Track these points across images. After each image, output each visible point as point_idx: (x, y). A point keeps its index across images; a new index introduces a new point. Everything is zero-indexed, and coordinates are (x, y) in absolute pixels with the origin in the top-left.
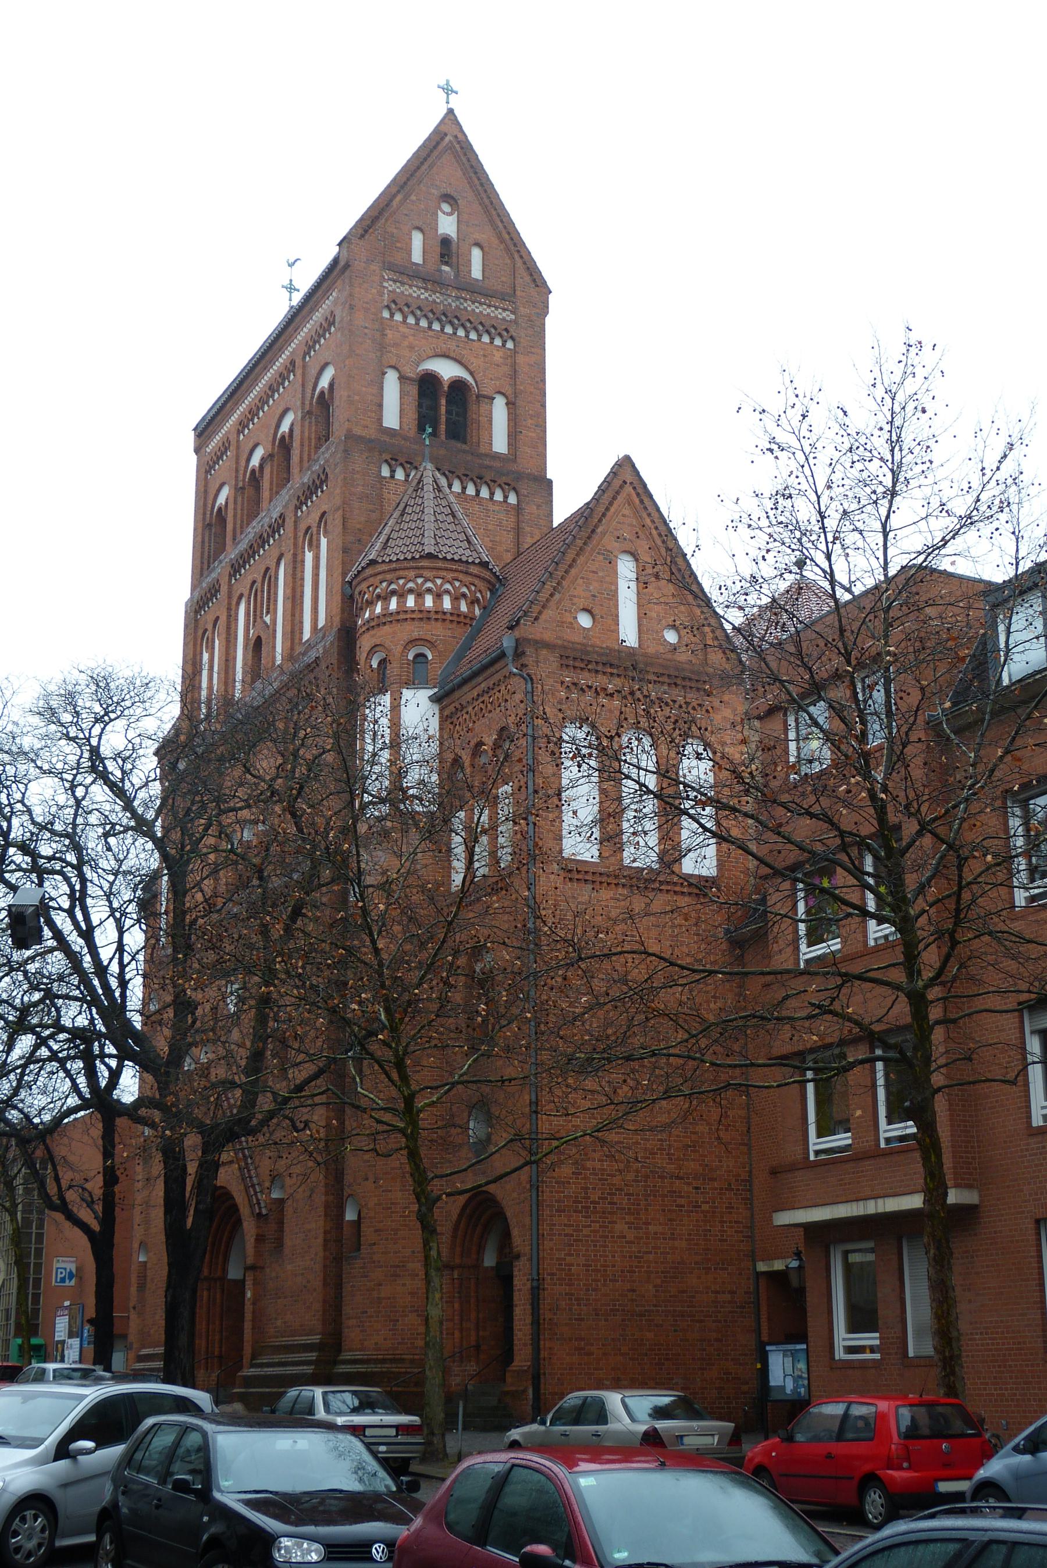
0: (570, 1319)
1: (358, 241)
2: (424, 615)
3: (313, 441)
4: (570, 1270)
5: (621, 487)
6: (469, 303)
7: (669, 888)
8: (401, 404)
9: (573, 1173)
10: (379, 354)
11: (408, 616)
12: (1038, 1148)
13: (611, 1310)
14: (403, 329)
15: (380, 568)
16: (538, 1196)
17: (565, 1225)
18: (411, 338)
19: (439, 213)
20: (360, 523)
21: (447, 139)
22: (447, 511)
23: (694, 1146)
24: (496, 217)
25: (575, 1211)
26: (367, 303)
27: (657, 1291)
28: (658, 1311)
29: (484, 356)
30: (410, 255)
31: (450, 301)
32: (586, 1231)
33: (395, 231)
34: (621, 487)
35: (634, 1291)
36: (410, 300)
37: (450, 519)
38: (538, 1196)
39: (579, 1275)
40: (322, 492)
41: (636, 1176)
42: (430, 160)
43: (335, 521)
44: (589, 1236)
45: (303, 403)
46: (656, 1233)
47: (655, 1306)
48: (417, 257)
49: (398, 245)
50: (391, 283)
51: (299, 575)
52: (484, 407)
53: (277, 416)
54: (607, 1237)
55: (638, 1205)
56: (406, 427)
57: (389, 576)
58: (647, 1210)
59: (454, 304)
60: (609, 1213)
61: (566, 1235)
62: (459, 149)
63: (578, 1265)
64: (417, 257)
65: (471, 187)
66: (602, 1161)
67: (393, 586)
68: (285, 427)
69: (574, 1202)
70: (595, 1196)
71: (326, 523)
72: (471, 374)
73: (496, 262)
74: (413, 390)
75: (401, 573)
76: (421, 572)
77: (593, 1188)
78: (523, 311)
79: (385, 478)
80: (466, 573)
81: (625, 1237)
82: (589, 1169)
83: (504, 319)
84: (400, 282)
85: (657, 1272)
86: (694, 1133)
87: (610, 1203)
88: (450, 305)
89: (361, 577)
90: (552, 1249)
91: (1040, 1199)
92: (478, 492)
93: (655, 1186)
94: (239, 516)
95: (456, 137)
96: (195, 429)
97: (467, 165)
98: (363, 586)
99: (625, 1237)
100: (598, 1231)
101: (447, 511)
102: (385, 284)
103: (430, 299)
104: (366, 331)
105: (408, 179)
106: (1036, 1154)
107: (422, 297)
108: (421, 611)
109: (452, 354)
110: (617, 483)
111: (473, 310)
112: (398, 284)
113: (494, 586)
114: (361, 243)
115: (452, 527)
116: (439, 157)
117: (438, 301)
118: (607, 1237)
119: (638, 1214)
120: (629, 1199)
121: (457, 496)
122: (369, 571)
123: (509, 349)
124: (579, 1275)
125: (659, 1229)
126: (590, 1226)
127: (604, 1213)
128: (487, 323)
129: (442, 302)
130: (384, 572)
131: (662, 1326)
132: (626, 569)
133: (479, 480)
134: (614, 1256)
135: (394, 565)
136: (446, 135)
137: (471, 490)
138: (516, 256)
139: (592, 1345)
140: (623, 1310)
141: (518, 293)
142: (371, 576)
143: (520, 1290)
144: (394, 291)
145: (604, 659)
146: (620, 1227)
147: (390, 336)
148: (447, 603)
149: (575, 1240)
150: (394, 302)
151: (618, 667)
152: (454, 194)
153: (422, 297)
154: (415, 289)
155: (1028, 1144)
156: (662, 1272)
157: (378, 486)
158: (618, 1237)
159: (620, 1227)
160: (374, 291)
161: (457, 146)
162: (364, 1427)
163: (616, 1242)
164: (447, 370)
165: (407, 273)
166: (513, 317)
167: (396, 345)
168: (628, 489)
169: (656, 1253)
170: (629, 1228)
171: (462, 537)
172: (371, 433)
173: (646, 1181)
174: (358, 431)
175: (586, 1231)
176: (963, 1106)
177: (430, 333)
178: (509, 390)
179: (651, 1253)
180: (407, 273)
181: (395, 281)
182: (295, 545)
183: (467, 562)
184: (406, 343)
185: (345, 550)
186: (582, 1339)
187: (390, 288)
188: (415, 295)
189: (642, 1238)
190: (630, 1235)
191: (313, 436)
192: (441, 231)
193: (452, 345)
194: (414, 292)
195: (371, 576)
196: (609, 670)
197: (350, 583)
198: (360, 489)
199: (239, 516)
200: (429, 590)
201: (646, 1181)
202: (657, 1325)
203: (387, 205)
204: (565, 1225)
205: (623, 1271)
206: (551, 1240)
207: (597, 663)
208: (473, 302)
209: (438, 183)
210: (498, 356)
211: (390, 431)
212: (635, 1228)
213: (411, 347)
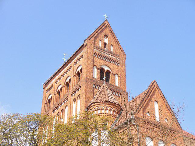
2: (106, 114)
3: (76, 81)
5: (154, 87)
11: (102, 114)
15: (96, 104)
21: (106, 25)
34: (154, 87)
40: (80, 89)
43: (83, 97)
45: (73, 74)
48: (100, 45)
51: (71, 109)
53: (66, 78)
57: (98, 106)
67: (99, 108)
68: (50, 98)
71: (63, 111)
72: (111, 69)
74: (99, 71)
75: (101, 105)
83: (117, 60)
89: (91, 106)
94: (54, 100)
98: (91, 108)
108: (106, 114)
109: (107, 65)
110: (153, 86)
128: (114, 60)
130: (97, 105)
132: (156, 106)
135: (99, 103)
142: (94, 106)
148: (111, 112)
150: (96, 53)
151: (156, 125)
165: (98, 48)
168: (155, 87)
172: (91, 78)
174: (88, 77)
180: (98, 48)
181: (96, 49)
182: (71, 103)
183: (114, 103)
185: (86, 102)
191: (76, 80)
195: (94, 106)
197: (87, 108)
199: (54, 100)
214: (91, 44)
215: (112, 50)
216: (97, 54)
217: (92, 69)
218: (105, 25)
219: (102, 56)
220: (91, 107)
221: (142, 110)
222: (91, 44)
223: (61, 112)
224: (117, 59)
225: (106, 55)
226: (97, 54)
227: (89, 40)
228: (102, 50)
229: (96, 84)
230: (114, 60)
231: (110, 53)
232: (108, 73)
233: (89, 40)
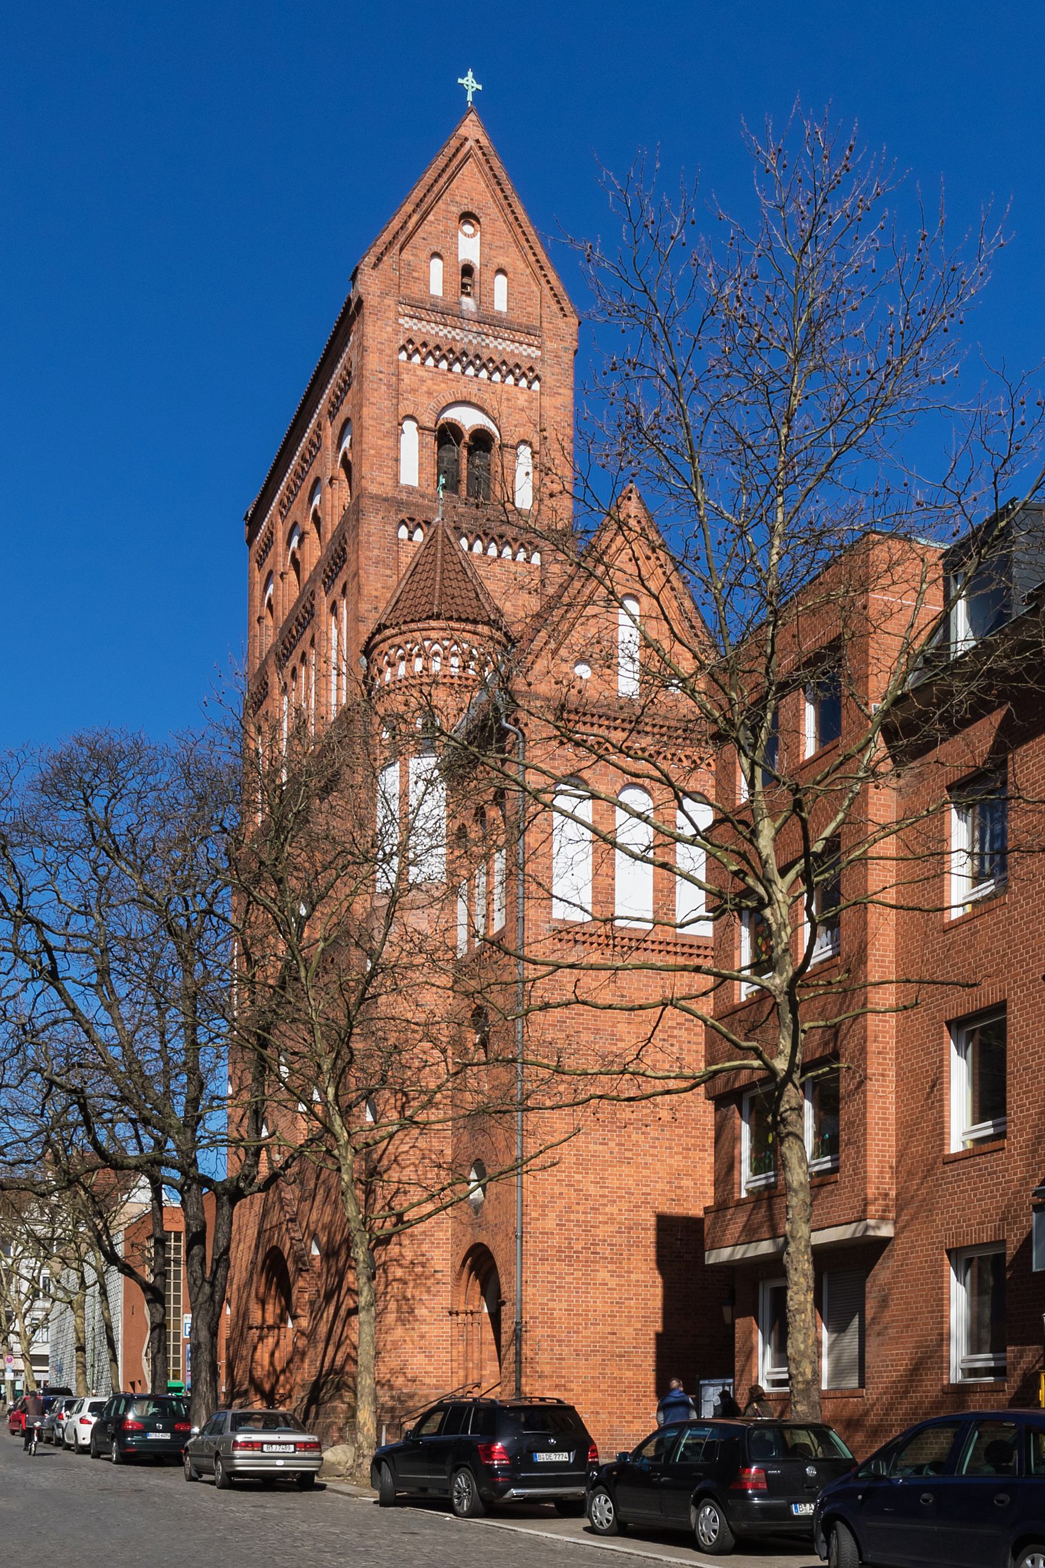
0: (551, 1359)
1: (371, 272)
4: (552, 1314)
6: (492, 338)
7: (661, 947)
8: (420, 458)
9: (557, 1225)
10: (395, 401)
12: (953, 1176)
13: (591, 1351)
14: (421, 372)
16: (522, 1246)
17: (548, 1273)
18: (430, 382)
19: (460, 234)
20: (376, 590)
21: (468, 145)
22: (458, 568)
23: (679, 1200)
24: (520, 236)
25: (558, 1260)
26: (381, 343)
27: (637, 1334)
28: (637, 1352)
29: (508, 400)
30: (428, 286)
31: (470, 337)
32: (569, 1279)
33: (411, 258)
35: (614, 1334)
36: (427, 338)
37: (460, 577)
38: (522, 1246)
39: (560, 1319)
41: (620, 1228)
42: (449, 171)
44: (572, 1283)
46: (637, 1281)
47: (634, 1348)
48: (436, 288)
49: (415, 274)
50: (407, 319)
52: (508, 457)
54: (589, 1284)
55: (621, 1254)
56: (425, 484)
58: (629, 1259)
59: (475, 342)
60: (592, 1262)
61: (549, 1282)
62: (481, 156)
63: (560, 1310)
64: (436, 288)
65: (495, 202)
66: (586, 1213)
69: (558, 1251)
70: (578, 1247)
72: (494, 420)
73: (522, 290)
74: (430, 440)
76: (428, 633)
77: (577, 1239)
78: (550, 345)
79: (403, 540)
80: (475, 633)
81: (607, 1284)
82: (573, 1221)
84: (416, 318)
85: (638, 1317)
86: (680, 1187)
87: (592, 1253)
88: (470, 342)
90: (534, 1295)
91: (951, 1229)
92: (500, 553)
93: (638, 1237)
95: (478, 141)
96: (245, 519)
97: (490, 175)
99: (607, 1284)
100: (581, 1279)
101: (458, 568)
102: (401, 321)
103: (450, 336)
104: (381, 376)
105: (425, 196)
106: (951, 1183)
107: (441, 334)
109: (474, 400)
111: (496, 347)
112: (415, 320)
113: (505, 647)
114: (374, 273)
115: (462, 585)
116: (459, 167)
117: (458, 338)
118: (589, 1284)
119: (620, 1263)
120: (612, 1250)
121: (479, 557)
122: (378, 638)
123: (534, 391)
124: (560, 1319)
125: (641, 1277)
126: (573, 1274)
127: (586, 1262)
128: (511, 362)
129: (462, 339)
131: (641, 1366)
133: (502, 540)
134: (595, 1302)
136: (466, 139)
137: (493, 551)
138: (543, 281)
139: (572, 1382)
140: (603, 1351)
141: (544, 325)
143: (506, 1332)
144: (410, 329)
145: (601, 711)
146: (603, 1275)
147: (406, 381)
149: (558, 1287)
152: (476, 212)
153: (441, 334)
154: (433, 325)
155: (944, 1172)
156: (643, 1317)
157: (395, 548)
158: (600, 1284)
159: (603, 1275)
160: (389, 329)
161: (479, 153)
162: (263, 1443)
163: (598, 1289)
164: (468, 419)
166: (539, 353)
167: (414, 391)
169: (637, 1299)
170: (612, 1276)
171: (472, 595)
172: (388, 491)
173: (629, 1233)
175: (569, 1279)
176: (883, 1135)
177: (450, 376)
178: (536, 440)
179: (632, 1299)
181: (412, 317)
184: (425, 389)
186: (564, 1377)
187: (406, 326)
188: (433, 332)
189: (623, 1285)
190: (613, 1283)
192: (460, 258)
193: (474, 388)
194: (432, 329)
196: (606, 723)
198: (376, 552)
200: (437, 654)
201: (629, 1233)
202: (635, 1365)
203: (402, 228)
204: (548, 1273)
205: (604, 1316)
206: (534, 1286)
207: (593, 716)
208: (496, 338)
209: (458, 199)
210: (522, 400)
211: (410, 490)
212: (617, 1276)
213: (429, 393)
214: (384, 294)
215: (501, 304)
216: (418, 342)
217: (390, 442)
218: (462, 145)
219: (445, 348)
220: (384, 641)
221: (629, 591)
222: (384, 294)
223: (918, 1336)
224: (526, 352)
225: (462, 338)
226: (418, 342)
227: (375, 266)
228: (447, 313)
229: (412, 519)
230: (511, 362)
231: (489, 321)
232: (481, 440)
233: (375, 266)
